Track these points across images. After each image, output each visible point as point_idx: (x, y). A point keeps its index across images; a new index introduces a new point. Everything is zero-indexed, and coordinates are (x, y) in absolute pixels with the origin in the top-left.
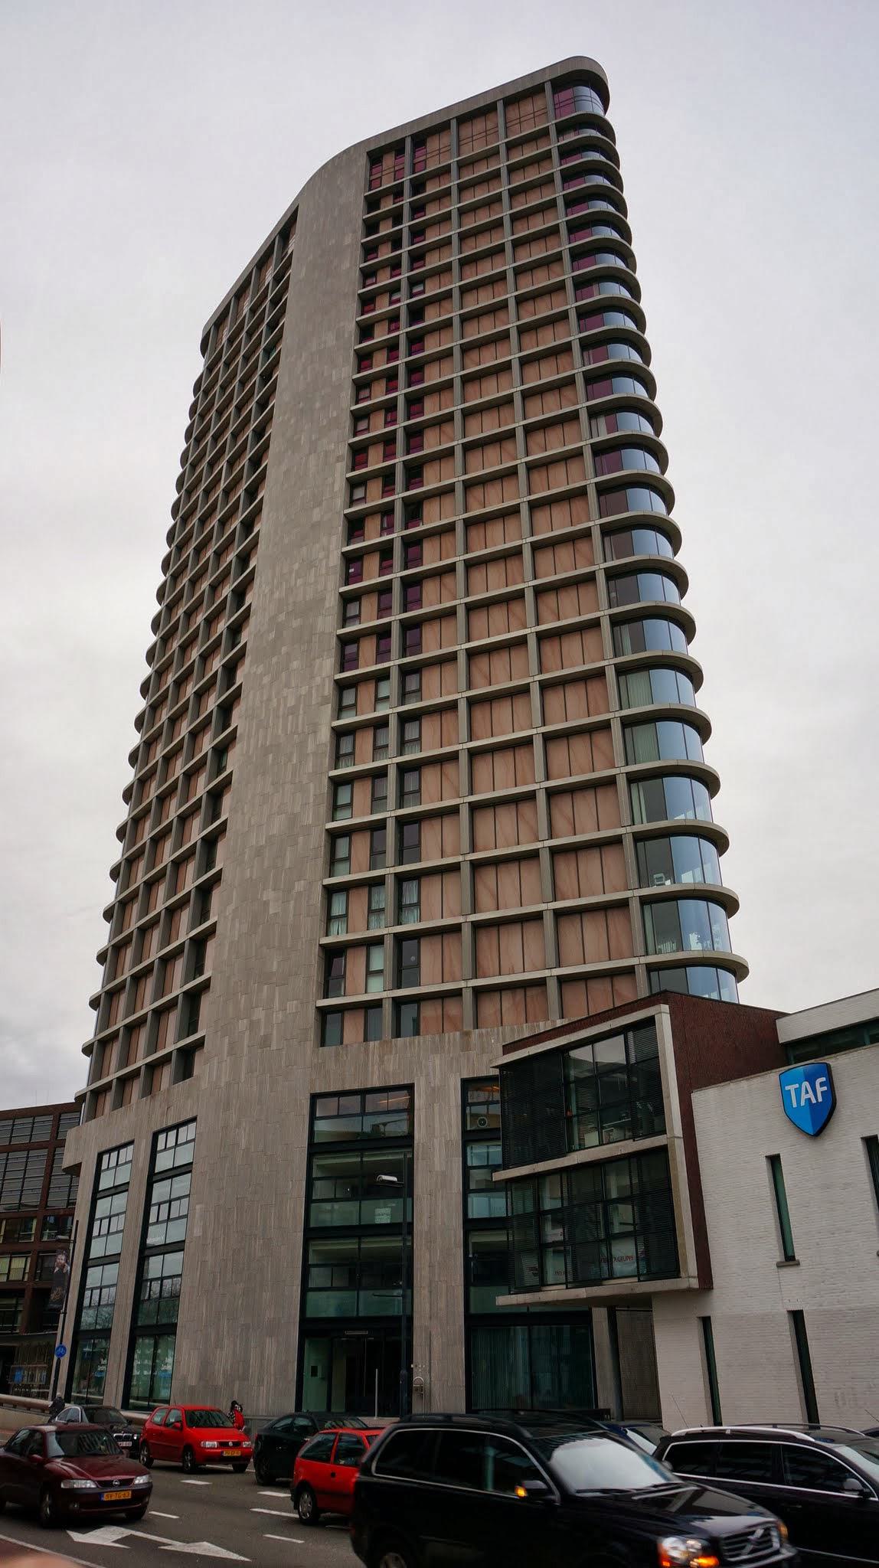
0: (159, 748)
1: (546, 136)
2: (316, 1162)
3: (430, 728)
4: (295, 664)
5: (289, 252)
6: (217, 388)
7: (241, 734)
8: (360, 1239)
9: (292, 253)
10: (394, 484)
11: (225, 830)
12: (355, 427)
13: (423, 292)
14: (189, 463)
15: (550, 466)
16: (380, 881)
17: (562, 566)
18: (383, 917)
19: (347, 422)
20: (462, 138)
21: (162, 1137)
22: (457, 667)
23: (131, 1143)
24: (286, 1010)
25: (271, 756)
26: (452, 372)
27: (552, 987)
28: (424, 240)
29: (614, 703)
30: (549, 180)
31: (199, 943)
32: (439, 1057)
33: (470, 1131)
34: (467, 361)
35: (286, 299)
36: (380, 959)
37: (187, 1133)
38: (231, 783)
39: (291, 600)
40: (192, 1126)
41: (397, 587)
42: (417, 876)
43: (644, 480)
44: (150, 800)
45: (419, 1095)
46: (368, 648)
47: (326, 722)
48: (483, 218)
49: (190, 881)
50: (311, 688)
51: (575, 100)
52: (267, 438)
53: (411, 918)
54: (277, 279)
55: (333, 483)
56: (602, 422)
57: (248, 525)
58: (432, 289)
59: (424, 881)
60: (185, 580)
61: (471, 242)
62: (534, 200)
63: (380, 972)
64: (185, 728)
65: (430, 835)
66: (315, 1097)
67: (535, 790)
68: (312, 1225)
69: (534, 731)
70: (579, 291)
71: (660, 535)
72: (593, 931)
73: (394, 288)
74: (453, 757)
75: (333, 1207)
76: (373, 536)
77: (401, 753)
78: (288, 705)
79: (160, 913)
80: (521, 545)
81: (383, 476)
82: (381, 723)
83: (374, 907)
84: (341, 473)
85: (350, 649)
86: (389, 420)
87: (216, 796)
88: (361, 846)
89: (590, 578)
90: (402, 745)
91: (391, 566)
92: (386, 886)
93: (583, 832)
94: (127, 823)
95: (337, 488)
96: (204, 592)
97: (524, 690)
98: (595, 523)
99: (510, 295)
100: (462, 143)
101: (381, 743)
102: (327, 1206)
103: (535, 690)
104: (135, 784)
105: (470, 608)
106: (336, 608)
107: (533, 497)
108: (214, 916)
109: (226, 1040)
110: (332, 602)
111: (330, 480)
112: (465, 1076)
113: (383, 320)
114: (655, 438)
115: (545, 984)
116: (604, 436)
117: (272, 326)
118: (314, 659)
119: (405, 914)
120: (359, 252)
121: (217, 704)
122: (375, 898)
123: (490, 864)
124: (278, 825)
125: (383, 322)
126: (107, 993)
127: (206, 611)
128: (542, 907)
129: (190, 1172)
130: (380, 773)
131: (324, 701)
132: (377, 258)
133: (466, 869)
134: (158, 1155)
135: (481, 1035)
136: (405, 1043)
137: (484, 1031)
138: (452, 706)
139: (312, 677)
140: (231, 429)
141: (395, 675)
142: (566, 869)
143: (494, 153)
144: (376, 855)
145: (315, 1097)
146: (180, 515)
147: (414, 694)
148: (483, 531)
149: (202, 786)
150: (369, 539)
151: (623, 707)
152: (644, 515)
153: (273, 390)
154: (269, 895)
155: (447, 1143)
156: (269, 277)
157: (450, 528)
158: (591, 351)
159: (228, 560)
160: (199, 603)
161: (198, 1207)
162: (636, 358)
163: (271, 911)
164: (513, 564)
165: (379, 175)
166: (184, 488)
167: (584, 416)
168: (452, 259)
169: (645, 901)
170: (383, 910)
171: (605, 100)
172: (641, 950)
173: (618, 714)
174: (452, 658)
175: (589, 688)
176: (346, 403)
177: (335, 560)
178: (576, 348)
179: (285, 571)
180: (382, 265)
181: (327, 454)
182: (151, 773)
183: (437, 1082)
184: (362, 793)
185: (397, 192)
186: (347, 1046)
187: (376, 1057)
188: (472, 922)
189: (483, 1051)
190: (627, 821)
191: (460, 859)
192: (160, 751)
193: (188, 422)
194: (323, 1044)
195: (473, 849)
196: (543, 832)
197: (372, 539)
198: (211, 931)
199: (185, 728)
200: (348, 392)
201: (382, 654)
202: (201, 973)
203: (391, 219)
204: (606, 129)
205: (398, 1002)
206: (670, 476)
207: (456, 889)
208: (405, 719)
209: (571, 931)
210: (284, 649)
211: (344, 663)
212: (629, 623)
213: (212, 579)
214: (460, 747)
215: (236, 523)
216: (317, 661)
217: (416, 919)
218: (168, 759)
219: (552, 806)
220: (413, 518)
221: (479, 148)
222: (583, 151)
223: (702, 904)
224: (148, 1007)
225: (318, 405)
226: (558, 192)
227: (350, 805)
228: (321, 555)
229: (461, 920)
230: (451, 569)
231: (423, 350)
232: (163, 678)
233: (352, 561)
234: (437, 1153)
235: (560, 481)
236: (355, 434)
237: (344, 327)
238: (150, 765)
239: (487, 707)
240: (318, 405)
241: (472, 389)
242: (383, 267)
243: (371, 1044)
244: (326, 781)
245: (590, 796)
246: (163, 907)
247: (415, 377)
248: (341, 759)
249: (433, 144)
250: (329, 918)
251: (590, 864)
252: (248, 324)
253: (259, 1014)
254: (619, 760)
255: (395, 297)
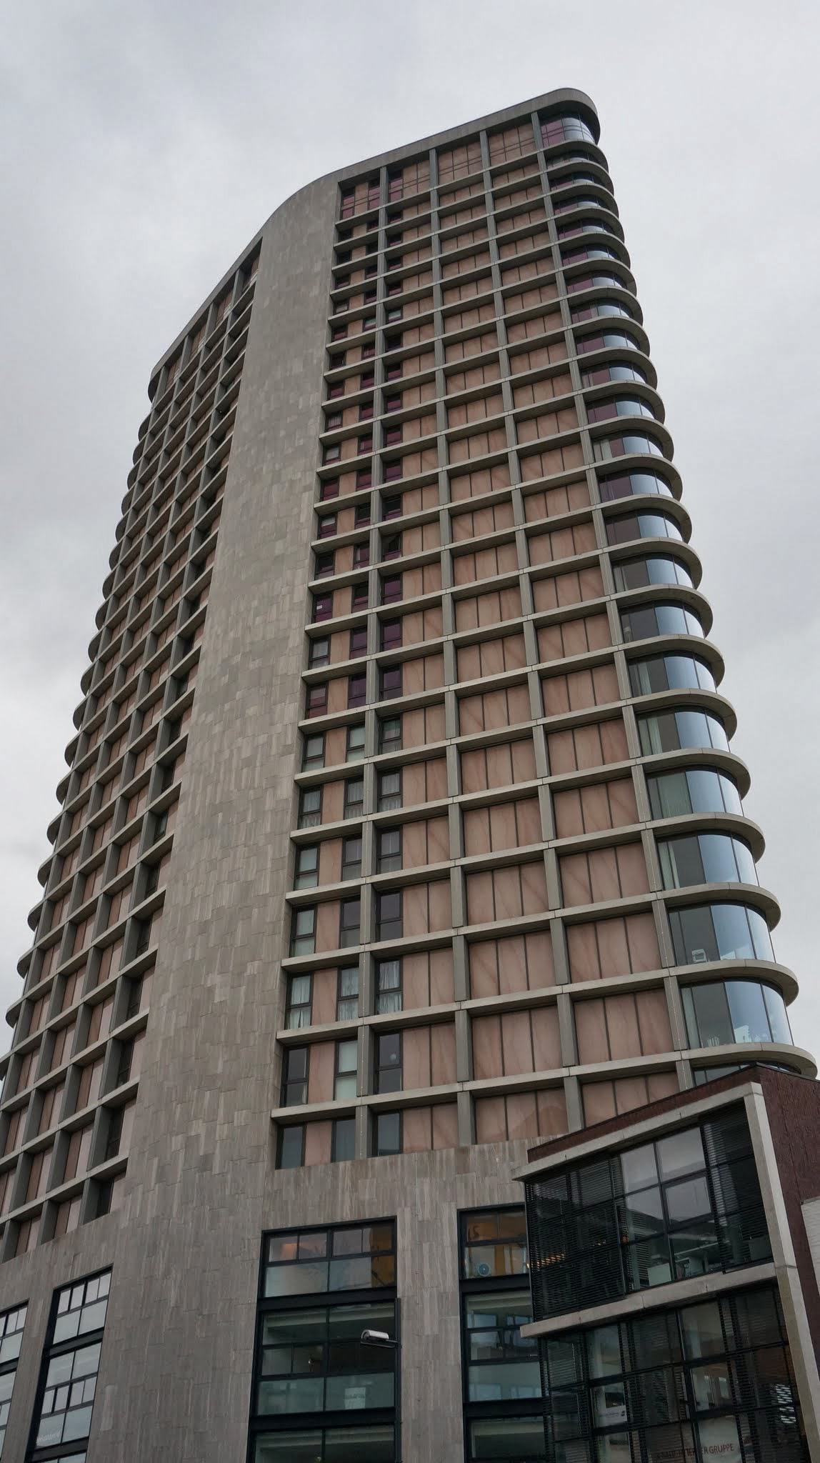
0: (76, 862)
1: (562, 341)
2: (267, 1325)
3: (412, 780)
4: (251, 711)
5: (251, 285)
6: (156, 479)
7: (184, 794)
8: (324, 1431)
9: (255, 284)
10: (367, 594)
11: (170, 850)
12: (327, 423)
13: (401, 318)
14: (143, 456)
15: (548, 493)
16: (351, 963)
17: (566, 599)
18: (356, 1006)
19: (316, 450)
20: (441, 169)
21: (65, 1296)
22: (457, 1109)
23: (25, 1304)
24: (233, 1122)
25: (220, 815)
26: (437, 502)
27: (572, 1090)
28: (402, 292)
29: (634, 749)
30: (536, 183)
31: (125, 1044)
32: (428, 1180)
33: (470, 1280)
34: (451, 387)
35: (247, 331)
36: (352, 1057)
37: (100, 1287)
38: (171, 850)
39: (248, 641)
40: (106, 1278)
41: (373, 625)
42: (397, 955)
43: (656, 505)
44: (71, 876)
45: (403, 1230)
46: (338, 692)
47: (289, 773)
48: (473, 352)
49: (107, 1029)
50: (270, 737)
51: (564, 130)
52: (233, 411)
53: (391, 1007)
54: (236, 313)
55: (299, 514)
56: (606, 446)
57: (187, 640)
58: (410, 315)
59: (408, 962)
60: (116, 665)
61: (459, 380)
62: (536, 332)
63: (353, 1073)
64: (108, 838)
65: (414, 906)
66: (267, 1236)
67: (542, 851)
68: (261, 1412)
69: (539, 782)
70: (592, 410)
71: (644, 408)
72: (619, 1019)
73: (369, 315)
74: (442, 813)
75: (288, 1386)
76: (344, 569)
77: (378, 809)
78: (243, 756)
79: (54, 1135)
80: (518, 576)
81: (366, 245)
82: (354, 776)
83: (345, 993)
84: (309, 502)
85: (317, 694)
86: (362, 448)
87: (152, 867)
88: (329, 918)
89: (600, 611)
90: (379, 861)
91: (367, 602)
92: (359, 1040)
93: (602, 899)
94: (32, 953)
95: (303, 519)
96: (137, 678)
97: (526, 736)
98: (603, 551)
99: (505, 380)
100: (441, 173)
101: (354, 798)
102: (281, 1385)
103: (539, 735)
104: (63, 817)
105: (459, 646)
106: (302, 647)
107: (529, 525)
108: (155, 944)
109: (156, 1161)
110: (297, 641)
111: (296, 511)
112: (463, 1206)
113: (357, 347)
114: (684, 544)
115: (549, 930)
116: (609, 459)
117: (218, 439)
118: (275, 704)
119: (383, 1001)
120: (329, 280)
121: (157, 760)
122: (346, 983)
123: (492, 1015)
124: (227, 896)
125: (355, 350)
126: (16, 1053)
127: (132, 741)
128: (556, 990)
129: (100, 1341)
130: (353, 834)
131: (286, 751)
132: (346, 337)
133: (459, 946)
134: (46, 1393)
135: (482, 1152)
136: (385, 1163)
137: (486, 1146)
138: (440, 755)
139: (272, 724)
140: (164, 558)
141: (370, 721)
142: (583, 942)
143: (479, 180)
144: (347, 930)
145: (267, 1236)
146: (107, 622)
147: (394, 743)
148: (472, 564)
149: (126, 910)
150: (331, 765)
151: (645, 752)
152: (651, 498)
153: (216, 514)
154: (215, 979)
155: (441, 1296)
156: (228, 312)
157: (434, 560)
158: (591, 375)
159: (168, 641)
160: (124, 729)
161: (108, 1389)
162: (665, 492)
163: (217, 1000)
164: (508, 598)
165: (352, 205)
166: (113, 593)
167: (586, 440)
168: (432, 284)
169: (686, 982)
170: (356, 997)
171: (595, 130)
172: (681, 1042)
173: (639, 761)
174: (439, 701)
175: (575, 535)
176: (315, 430)
177: (301, 596)
178: (574, 370)
179: (242, 608)
180: (349, 404)
181: (292, 482)
182: (66, 891)
183: (427, 1215)
184: (331, 856)
185: (372, 221)
186: (309, 1167)
187: (348, 1182)
188: (468, 1010)
189: (485, 1174)
190: (656, 884)
191: (452, 933)
192: (76, 866)
193: (108, 571)
194: (278, 1165)
195: (468, 921)
196: (554, 900)
197: (335, 764)
198: (141, 1028)
199: (108, 838)
200: (316, 421)
201: (356, 698)
202: (125, 1080)
203: (358, 407)
204: (599, 157)
205: (375, 1112)
206: (695, 544)
207: (446, 971)
208: (383, 770)
209: (592, 1021)
210: (238, 695)
211: (310, 709)
212: (658, 716)
213: (142, 701)
214: (449, 801)
215: (172, 637)
216: (279, 706)
217: (397, 1008)
218: (86, 875)
219: (563, 870)
220: (390, 551)
221: (460, 176)
222: (585, 225)
223: (756, 986)
224: (56, 1125)
225: (282, 433)
226: (558, 268)
227: (316, 872)
228: (284, 590)
229: (453, 1007)
230: (436, 603)
231: (401, 407)
232: (85, 778)
233: (321, 597)
234: (427, 1311)
235: (560, 508)
236: (324, 462)
237: (312, 354)
238: (63, 883)
239: (481, 755)
240: (282, 433)
241: (464, 567)
242: (351, 406)
243: (341, 1164)
244: (287, 843)
245: (609, 857)
246: (81, 1001)
247: (391, 471)
248: (305, 818)
249: (410, 175)
250: (289, 1008)
251: (613, 938)
252: (203, 361)
253: (199, 1128)
254: (644, 813)
255: (369, 324)
